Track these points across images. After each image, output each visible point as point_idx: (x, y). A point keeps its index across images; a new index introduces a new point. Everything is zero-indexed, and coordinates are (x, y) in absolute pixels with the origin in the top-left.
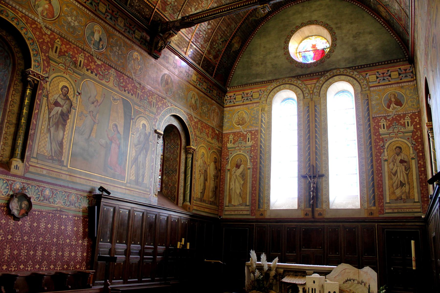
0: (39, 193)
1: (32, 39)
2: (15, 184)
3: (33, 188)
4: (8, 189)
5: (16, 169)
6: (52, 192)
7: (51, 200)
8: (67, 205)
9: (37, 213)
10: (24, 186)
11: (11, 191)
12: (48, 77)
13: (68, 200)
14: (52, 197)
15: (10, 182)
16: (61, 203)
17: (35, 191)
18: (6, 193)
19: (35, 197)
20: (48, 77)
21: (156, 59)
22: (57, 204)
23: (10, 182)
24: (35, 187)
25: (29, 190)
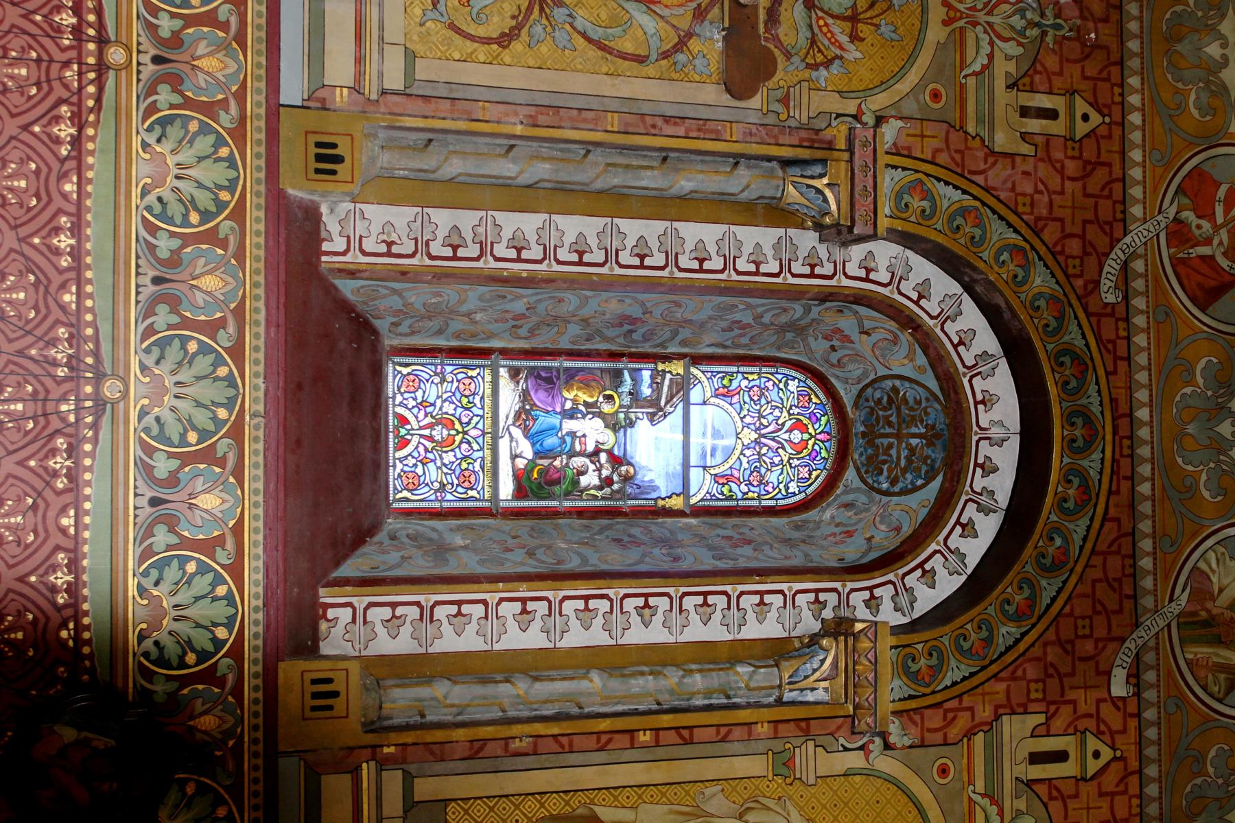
0: (192, 437)
1: (1089, 422)
2: (223, 47)
3: (219, 393)
4: (183, 665)
5: (320, 158)
6: (221, 324)
7: (165, 95)
8: (152, 230)
9: (64, 241)
10: (224, 104)
11: (176, 243)
12: (887, 746)
13: (187, 240)
14: (186, 323)
15: (224, 446)
16: (157, 399)
17: (199, 405)
18: (154, 652)
19: (167, 416)
20: (887, 746)
21: (1031, 754)
22: (143, 368)
23: (224, 446)
24: (229, 404)
25: (204, 144)
